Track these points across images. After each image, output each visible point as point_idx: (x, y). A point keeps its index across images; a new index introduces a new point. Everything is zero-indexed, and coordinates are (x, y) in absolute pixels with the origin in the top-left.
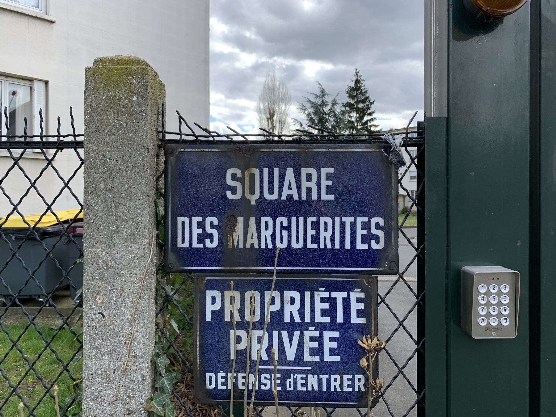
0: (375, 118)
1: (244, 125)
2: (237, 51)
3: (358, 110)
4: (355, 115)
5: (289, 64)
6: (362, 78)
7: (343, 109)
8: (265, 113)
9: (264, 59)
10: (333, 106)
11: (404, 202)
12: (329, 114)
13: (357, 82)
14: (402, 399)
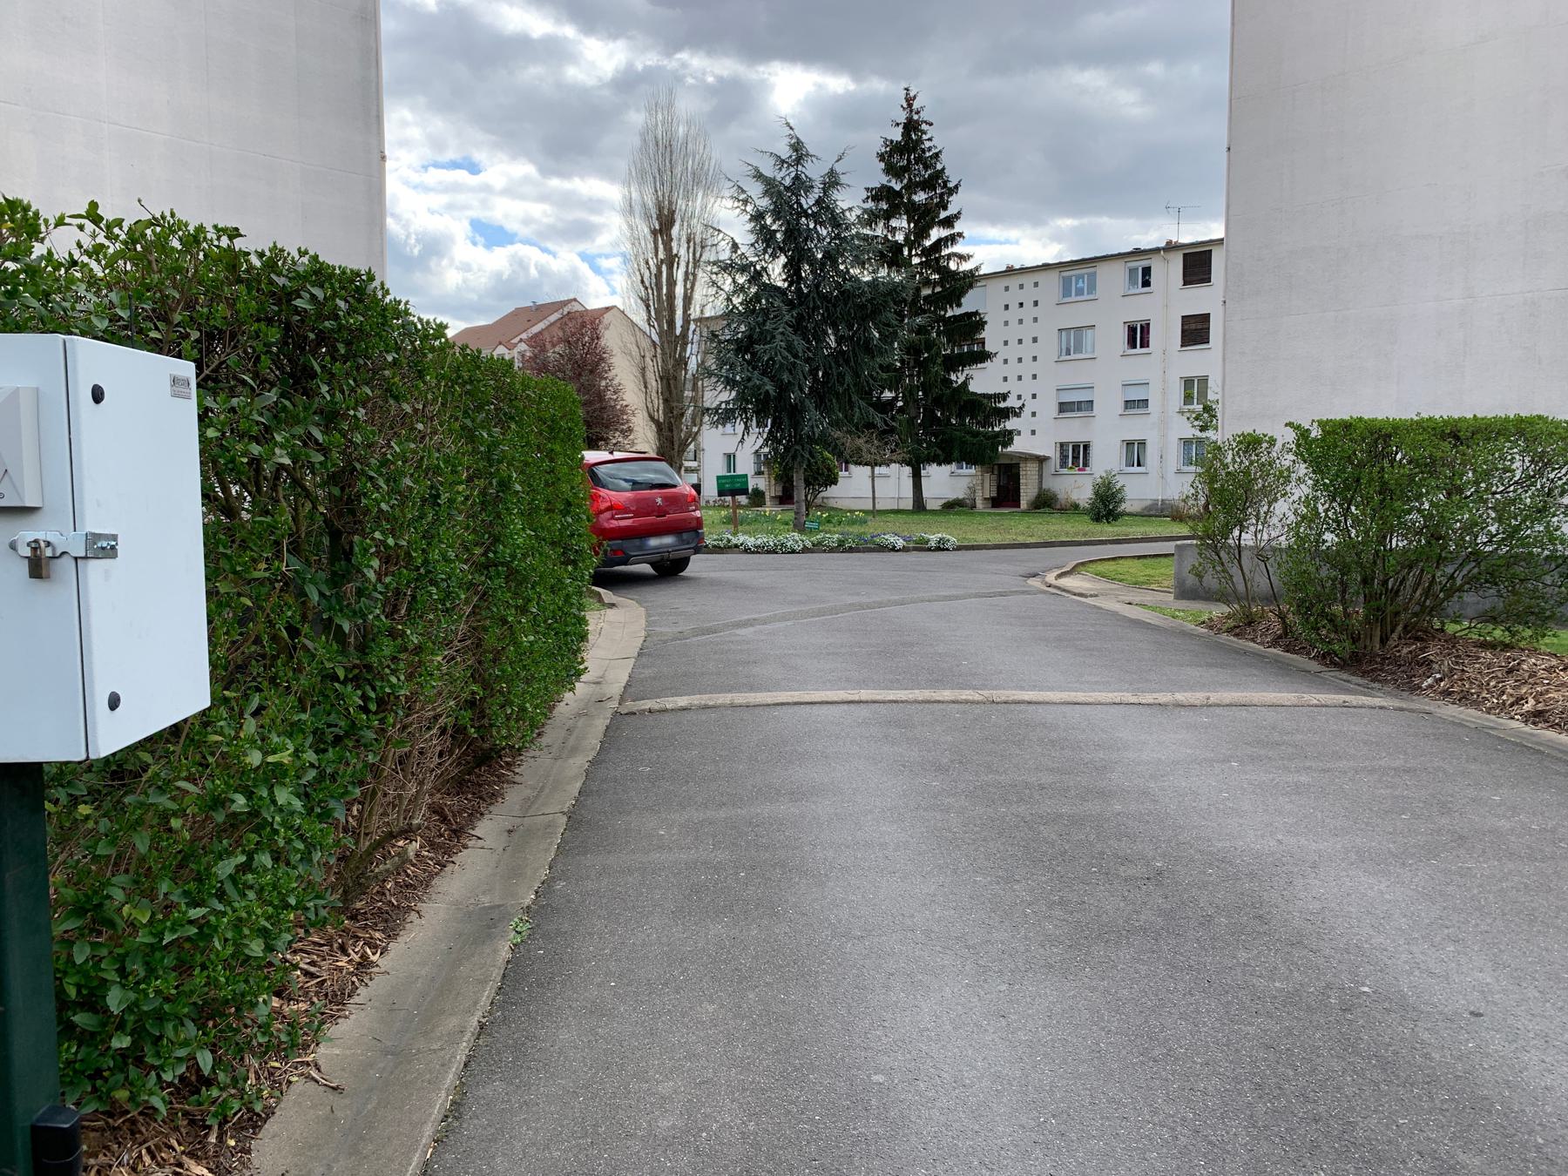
0: (960, 235)
1: (600, 256)
2: (569, 31)
3: (913, 211)
4: (905, 224)
5: (725, 73)
6: (924, 116)
7: (870, 204)
8: (647, 217)
9: (650, 59)
10: (825, 191)
11: (1041, 476)
12: (814, 215)
13: (911, 126)
14: (751, 1126)
